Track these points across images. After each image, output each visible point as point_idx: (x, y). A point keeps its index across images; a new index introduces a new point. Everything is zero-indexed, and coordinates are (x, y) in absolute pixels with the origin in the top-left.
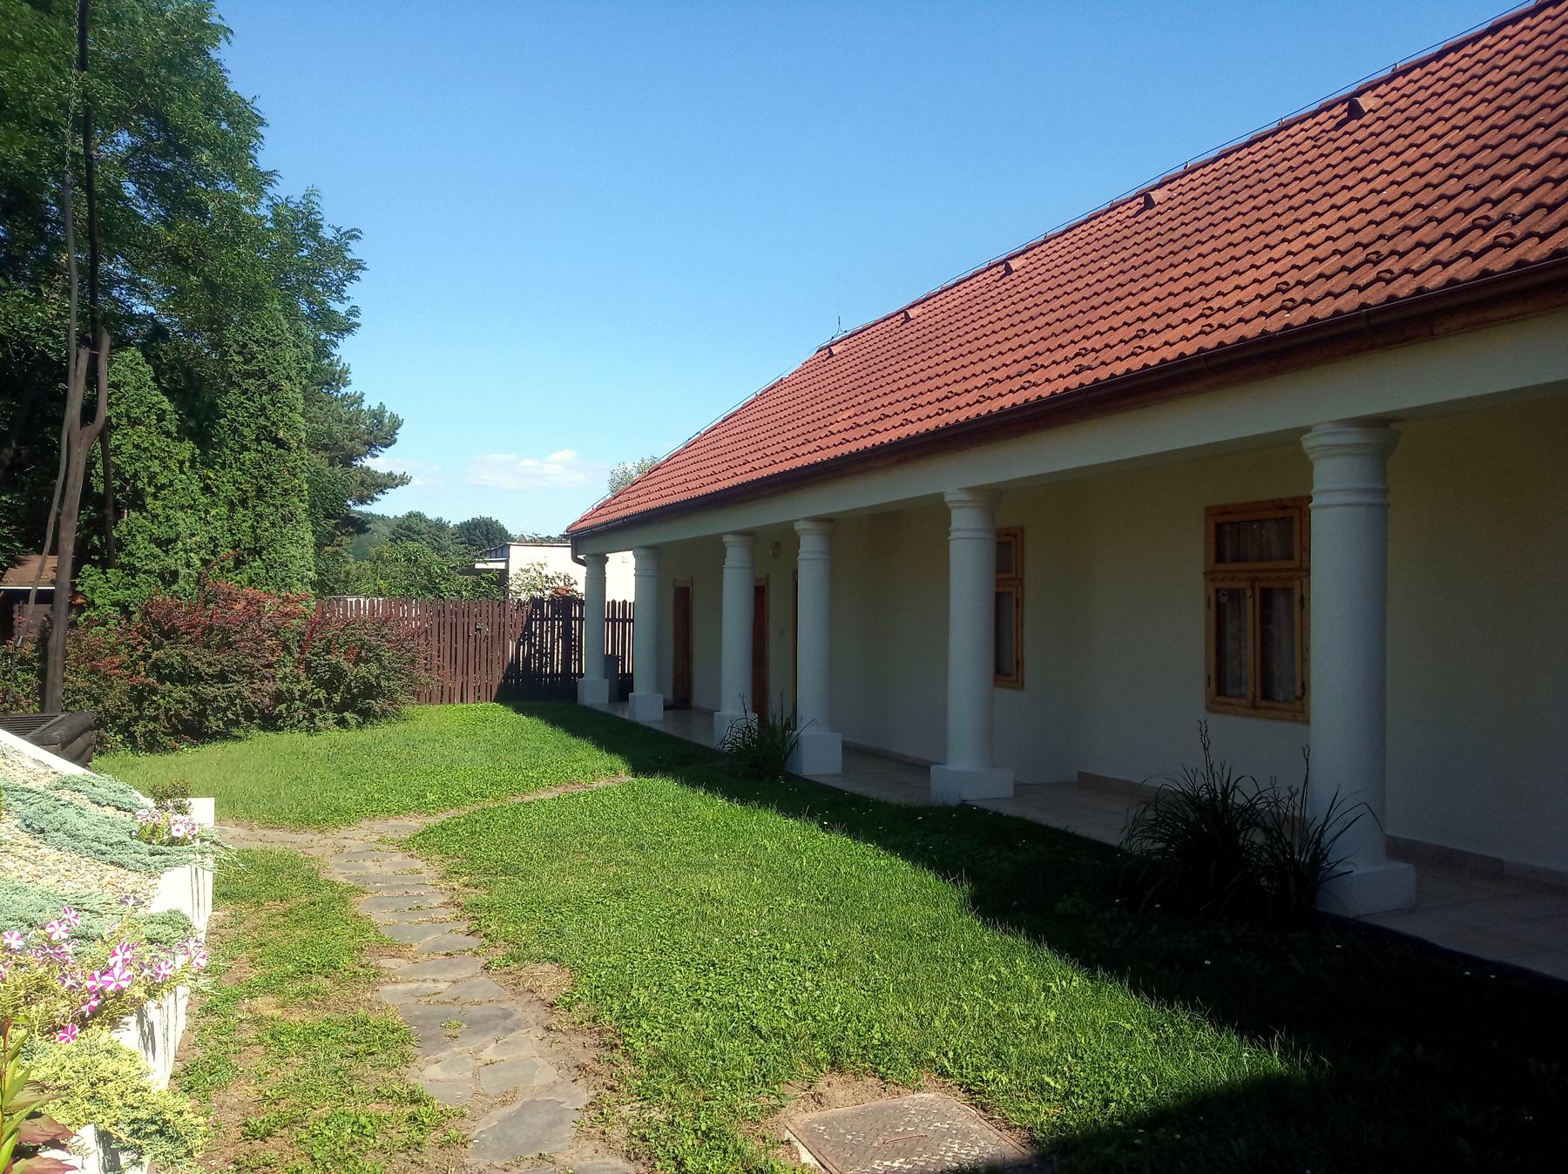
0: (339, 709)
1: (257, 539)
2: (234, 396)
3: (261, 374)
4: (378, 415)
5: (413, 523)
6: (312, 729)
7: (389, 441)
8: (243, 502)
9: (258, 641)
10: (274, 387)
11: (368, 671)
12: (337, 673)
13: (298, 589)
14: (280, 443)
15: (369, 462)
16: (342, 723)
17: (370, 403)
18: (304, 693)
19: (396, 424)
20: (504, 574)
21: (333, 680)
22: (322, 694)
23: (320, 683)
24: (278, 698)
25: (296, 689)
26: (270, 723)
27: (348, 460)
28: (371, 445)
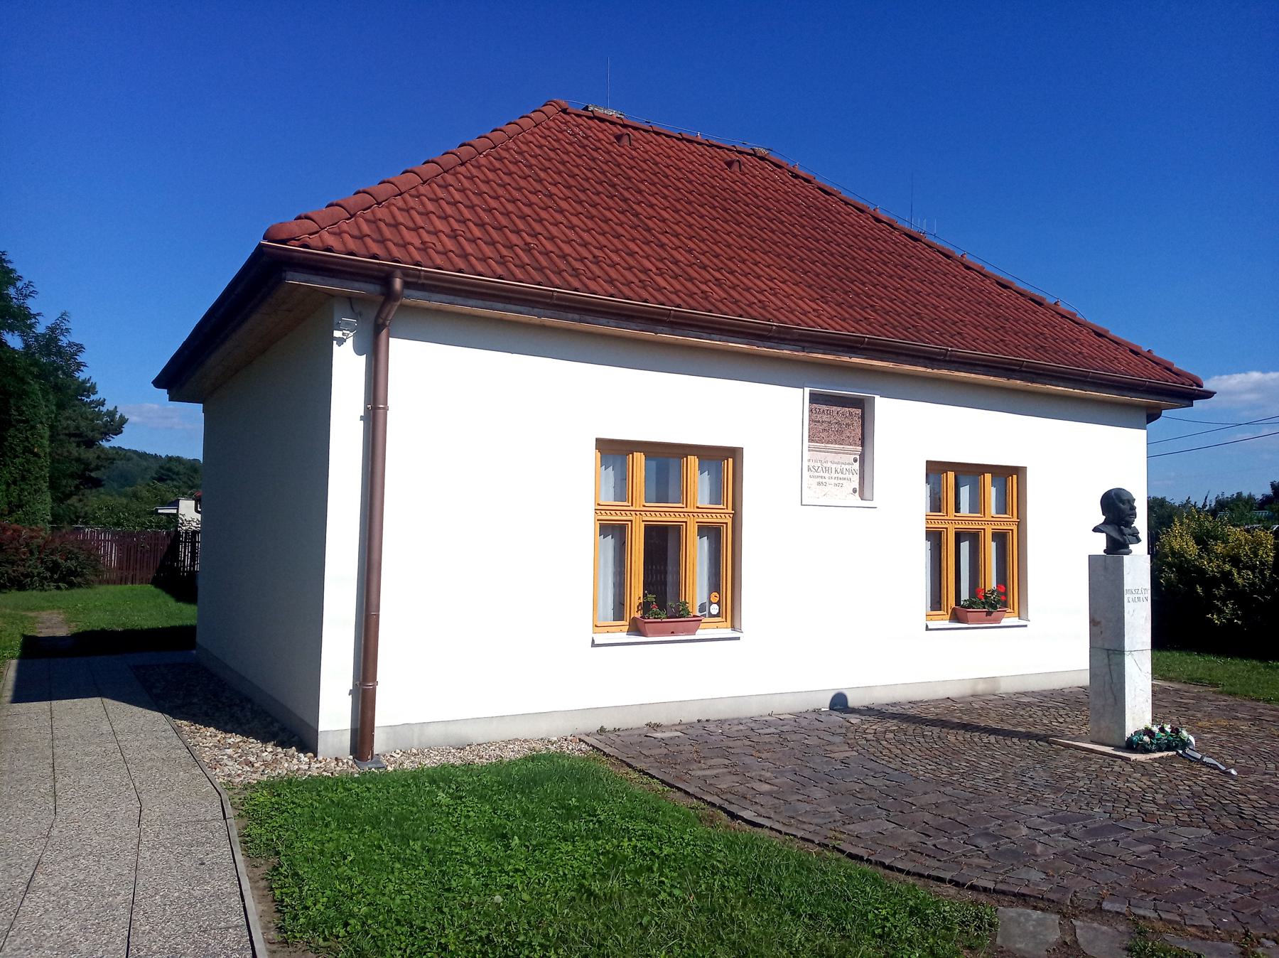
0: (56, 581)
1: (20, 500)
2: (12, 431)
3: (27, 421)
4: (111, 414)
5: (173, 465)
6: (43, 589)
7: (118, 431)
8: (15, 483)
9: (17, 549)
10: (33, 427)
11: (71, 564)
12: (55, 563)
13: (41, 525)
14: (36, 455)
15: (105, 444)
16: (58, 588)
17: (109, 406)
18: (39, 574)
19: (123, 421)
20: (176, 516)
21: (55, 567)
22: (48, 574)
23: (47, 569)
24: (27, 576)
25: (35, 571)
26: (22, 587)
27: (90, 443)
28: (106, 434)
